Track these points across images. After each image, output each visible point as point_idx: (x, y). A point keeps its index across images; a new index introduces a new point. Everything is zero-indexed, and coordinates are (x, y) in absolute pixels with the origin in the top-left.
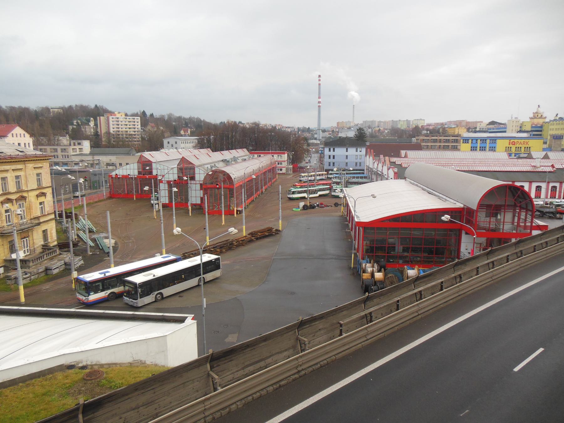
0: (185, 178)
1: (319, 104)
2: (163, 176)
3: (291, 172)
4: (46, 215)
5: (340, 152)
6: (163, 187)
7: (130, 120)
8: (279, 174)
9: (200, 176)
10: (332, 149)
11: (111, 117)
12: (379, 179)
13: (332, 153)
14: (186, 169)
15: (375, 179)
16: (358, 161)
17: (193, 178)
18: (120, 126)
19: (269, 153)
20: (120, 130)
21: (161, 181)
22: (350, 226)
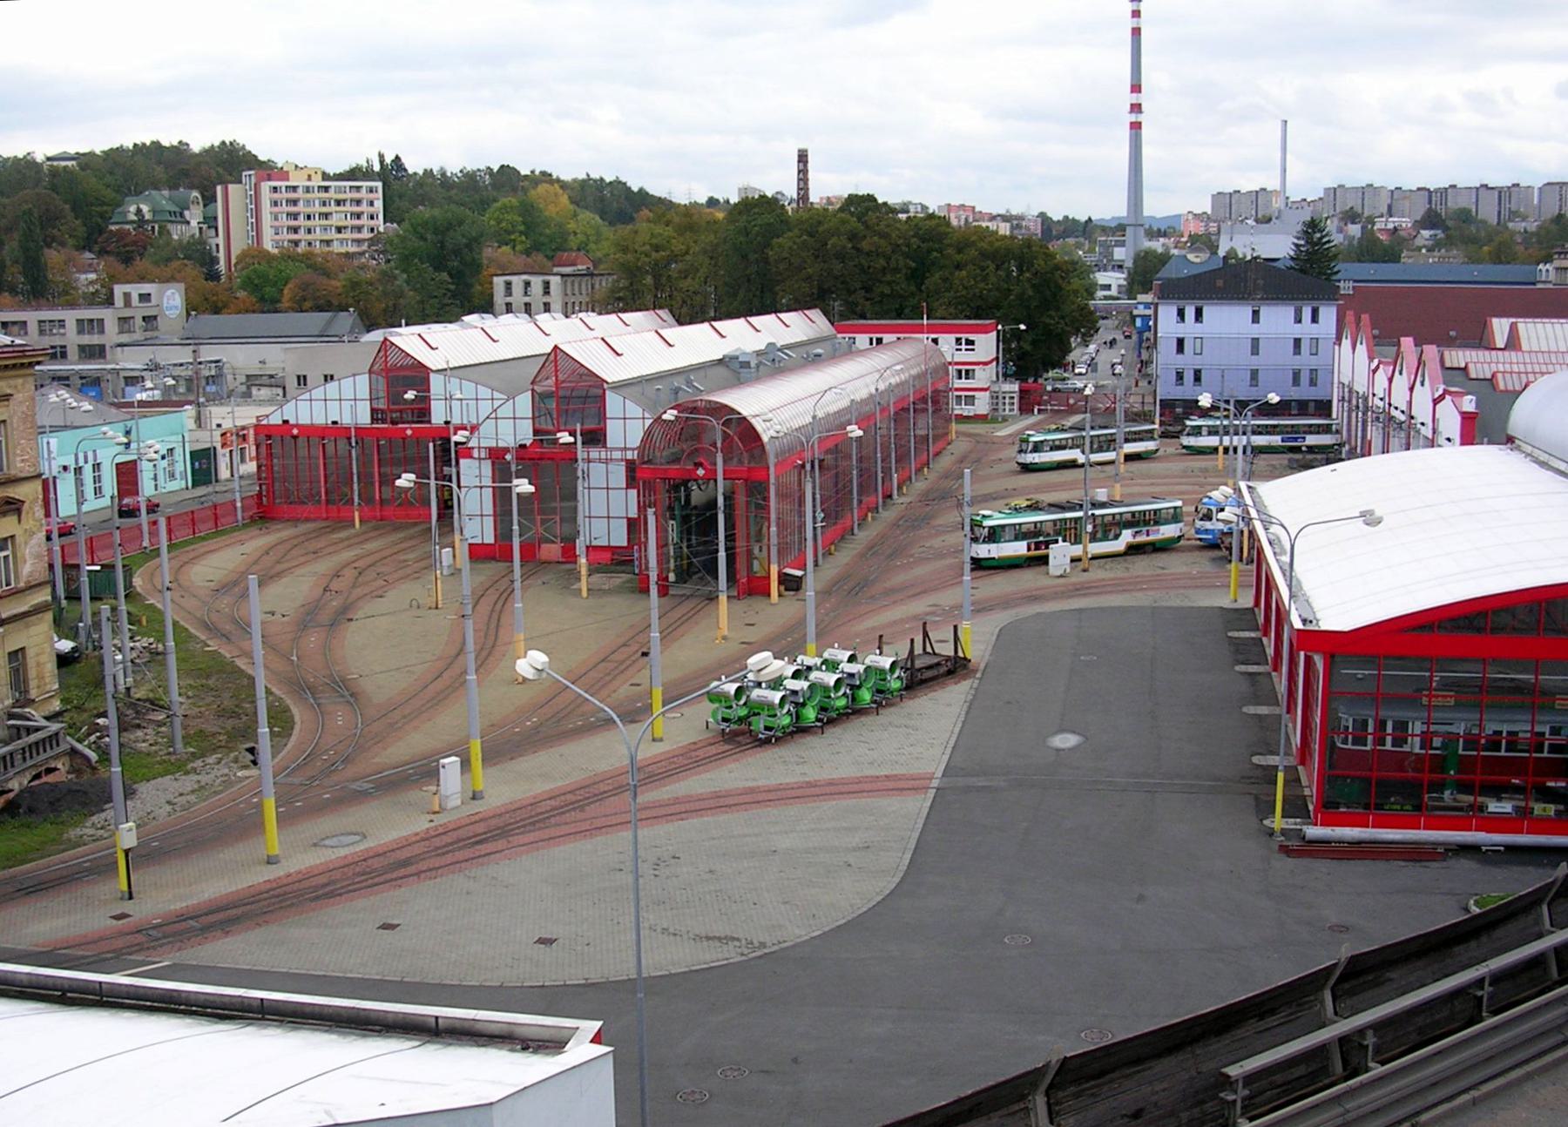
0: (565, 438)
1: (1133, 118)
2: (474, 429)
3: (1011, 408)
4: (22, 591)
5: (1226, 322)
6: (473, 476)
7: (341, 196)
8: (962, 419)
9: (627, 427)
10: (1190, 312)
11: (266, 186)
12: (1394, 442)
13: (1189, 328)
14: (571, 396)
15: (1377, 443)
16: (1305, 361)
17: (595, 437)
18: (301, 221)
19: (920, 329)
20: (302, 235)
21: (464, 451)
22: (1270, 651)
